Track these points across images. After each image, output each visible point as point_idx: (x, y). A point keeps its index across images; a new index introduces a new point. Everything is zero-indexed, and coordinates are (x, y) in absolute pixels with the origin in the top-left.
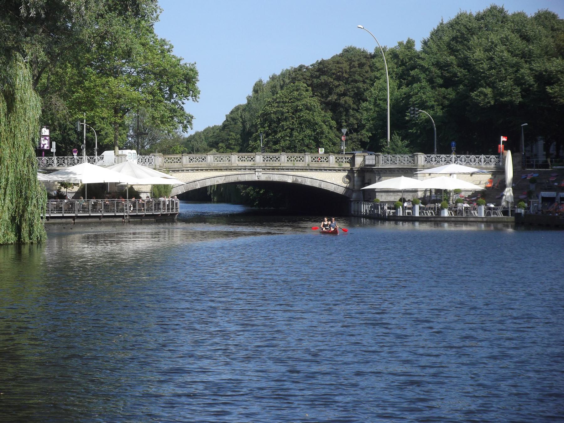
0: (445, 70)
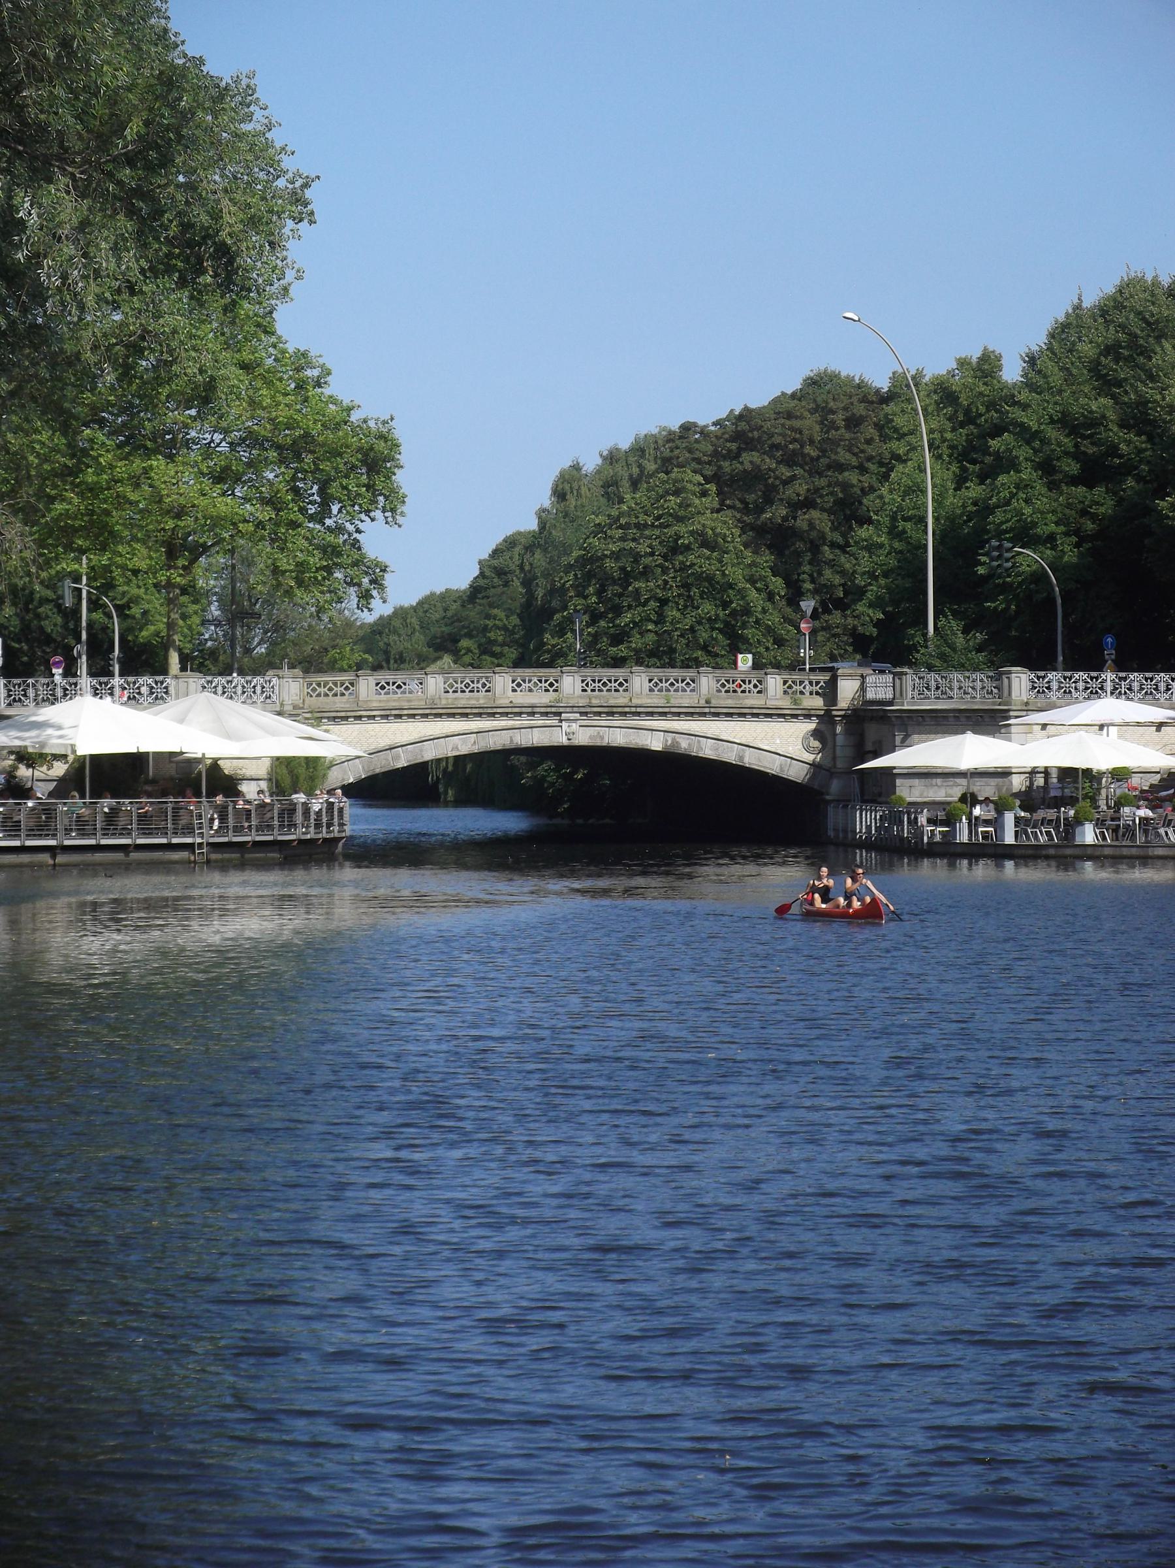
0: (1084, 437)
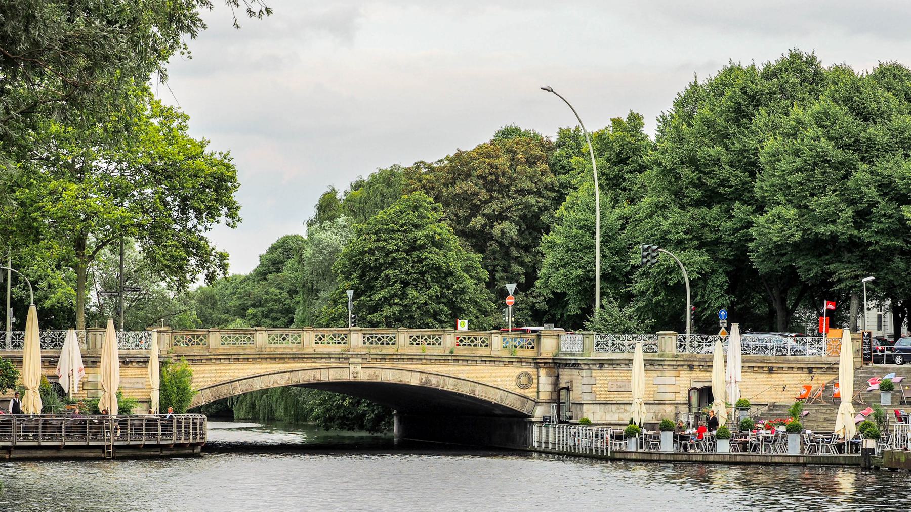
0: (705, 173)
